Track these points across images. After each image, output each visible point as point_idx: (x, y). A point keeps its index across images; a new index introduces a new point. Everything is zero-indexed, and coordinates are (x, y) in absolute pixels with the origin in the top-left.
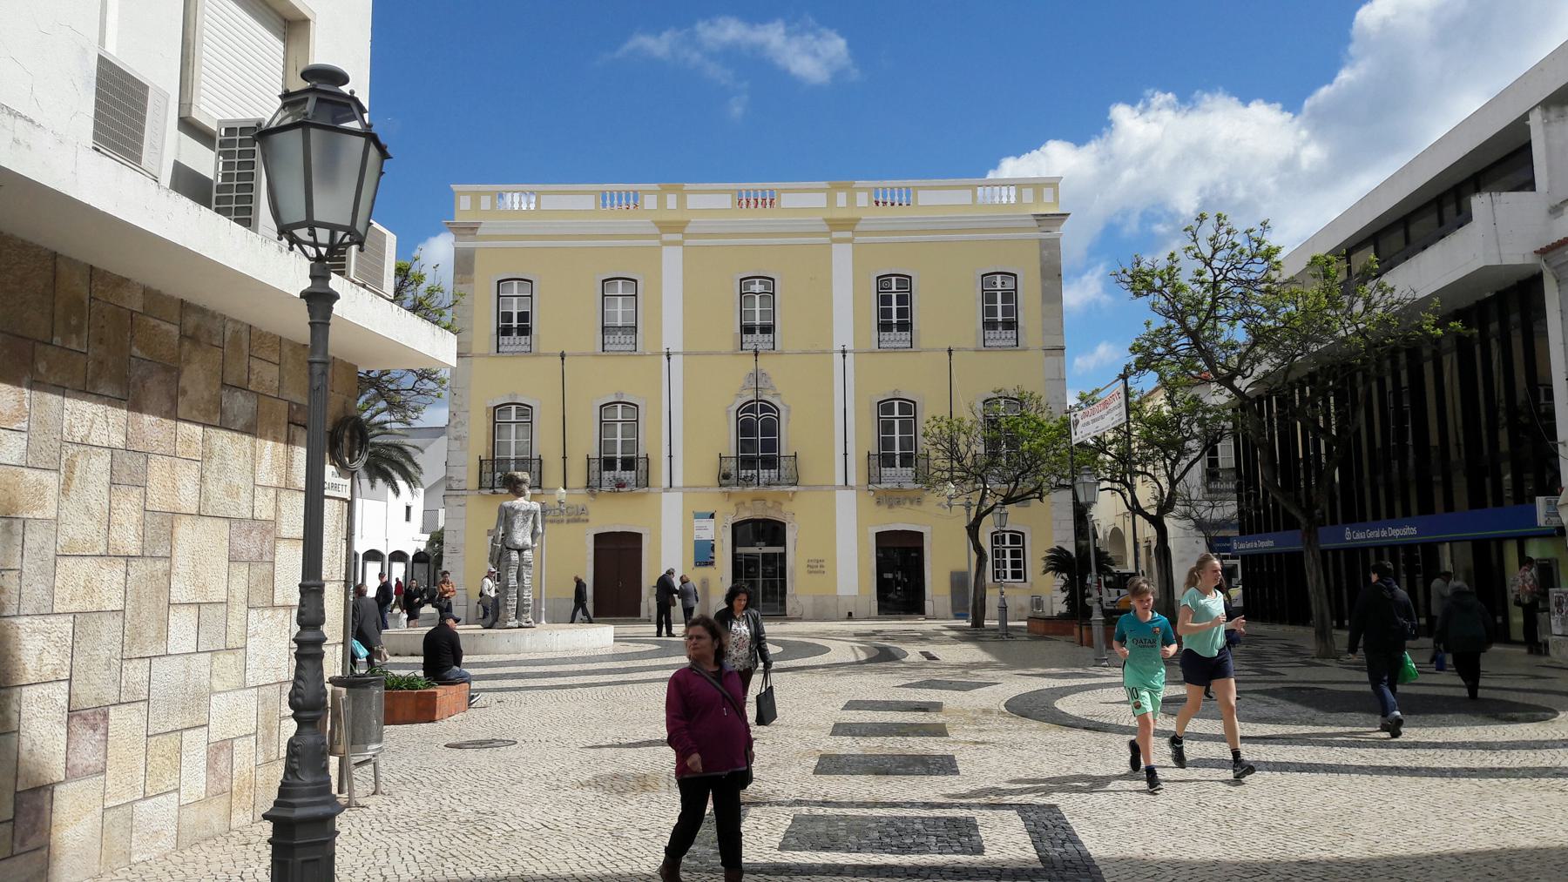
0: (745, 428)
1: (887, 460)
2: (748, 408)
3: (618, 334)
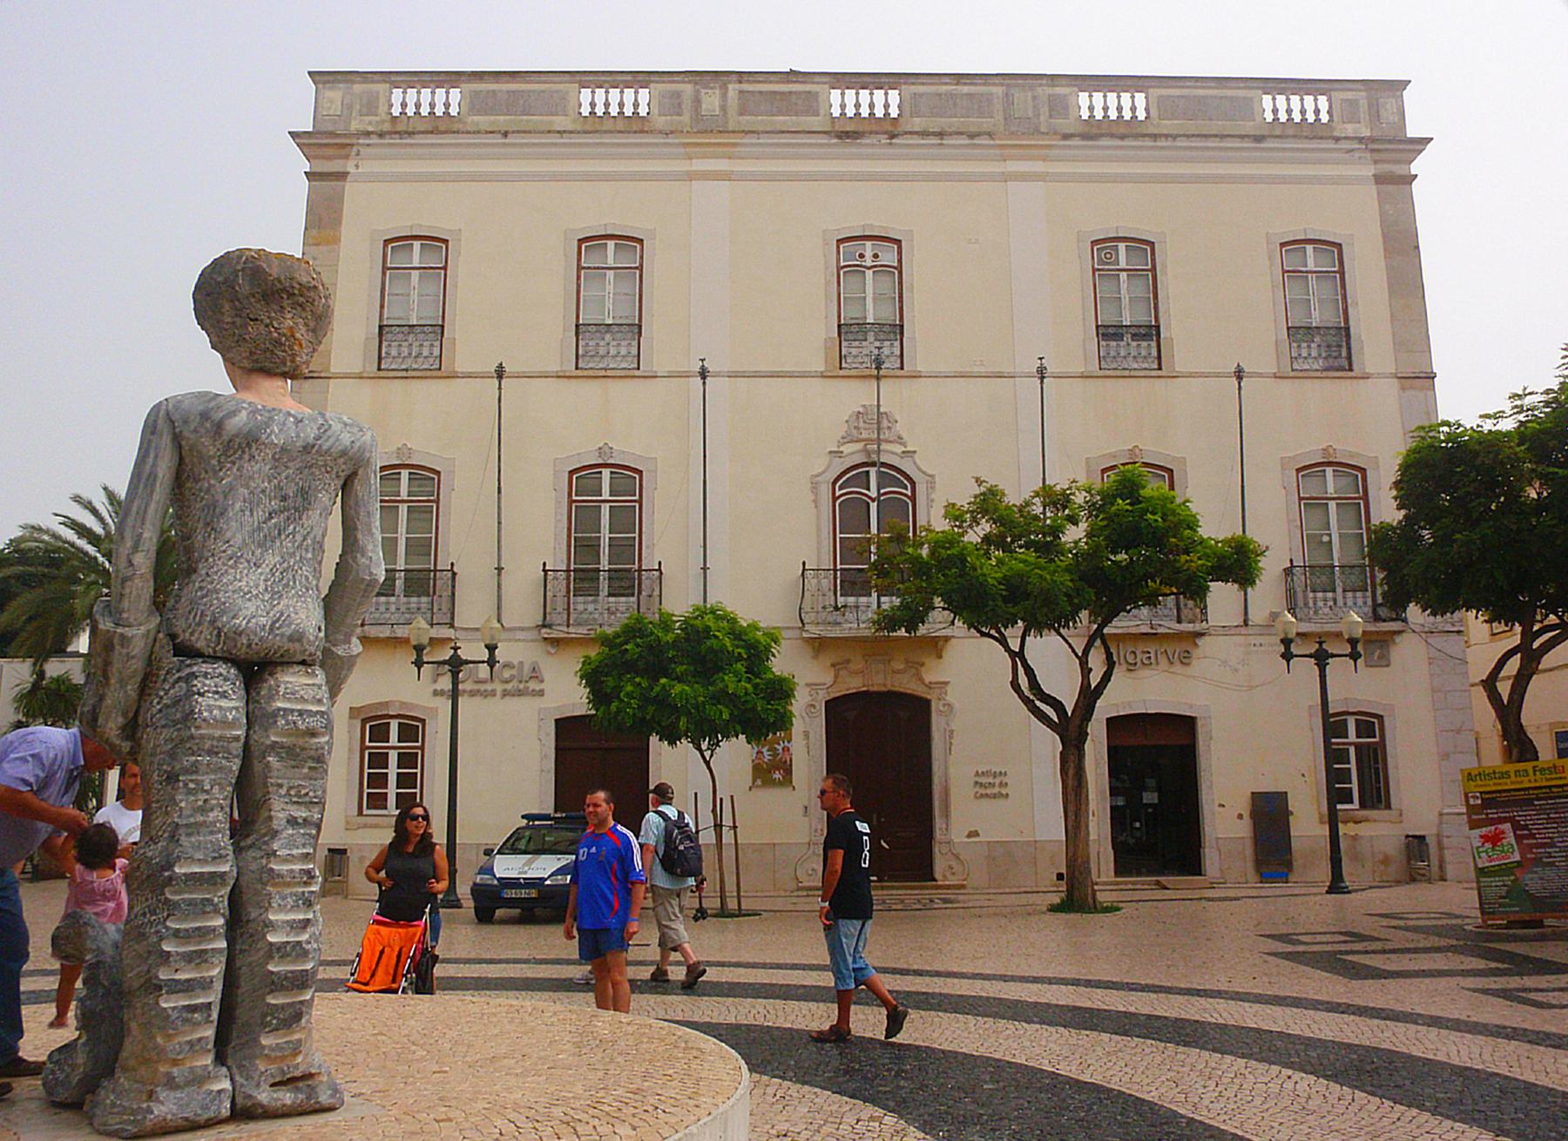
0: (581, 517)
2: (856, 475)
3: (606, 344)
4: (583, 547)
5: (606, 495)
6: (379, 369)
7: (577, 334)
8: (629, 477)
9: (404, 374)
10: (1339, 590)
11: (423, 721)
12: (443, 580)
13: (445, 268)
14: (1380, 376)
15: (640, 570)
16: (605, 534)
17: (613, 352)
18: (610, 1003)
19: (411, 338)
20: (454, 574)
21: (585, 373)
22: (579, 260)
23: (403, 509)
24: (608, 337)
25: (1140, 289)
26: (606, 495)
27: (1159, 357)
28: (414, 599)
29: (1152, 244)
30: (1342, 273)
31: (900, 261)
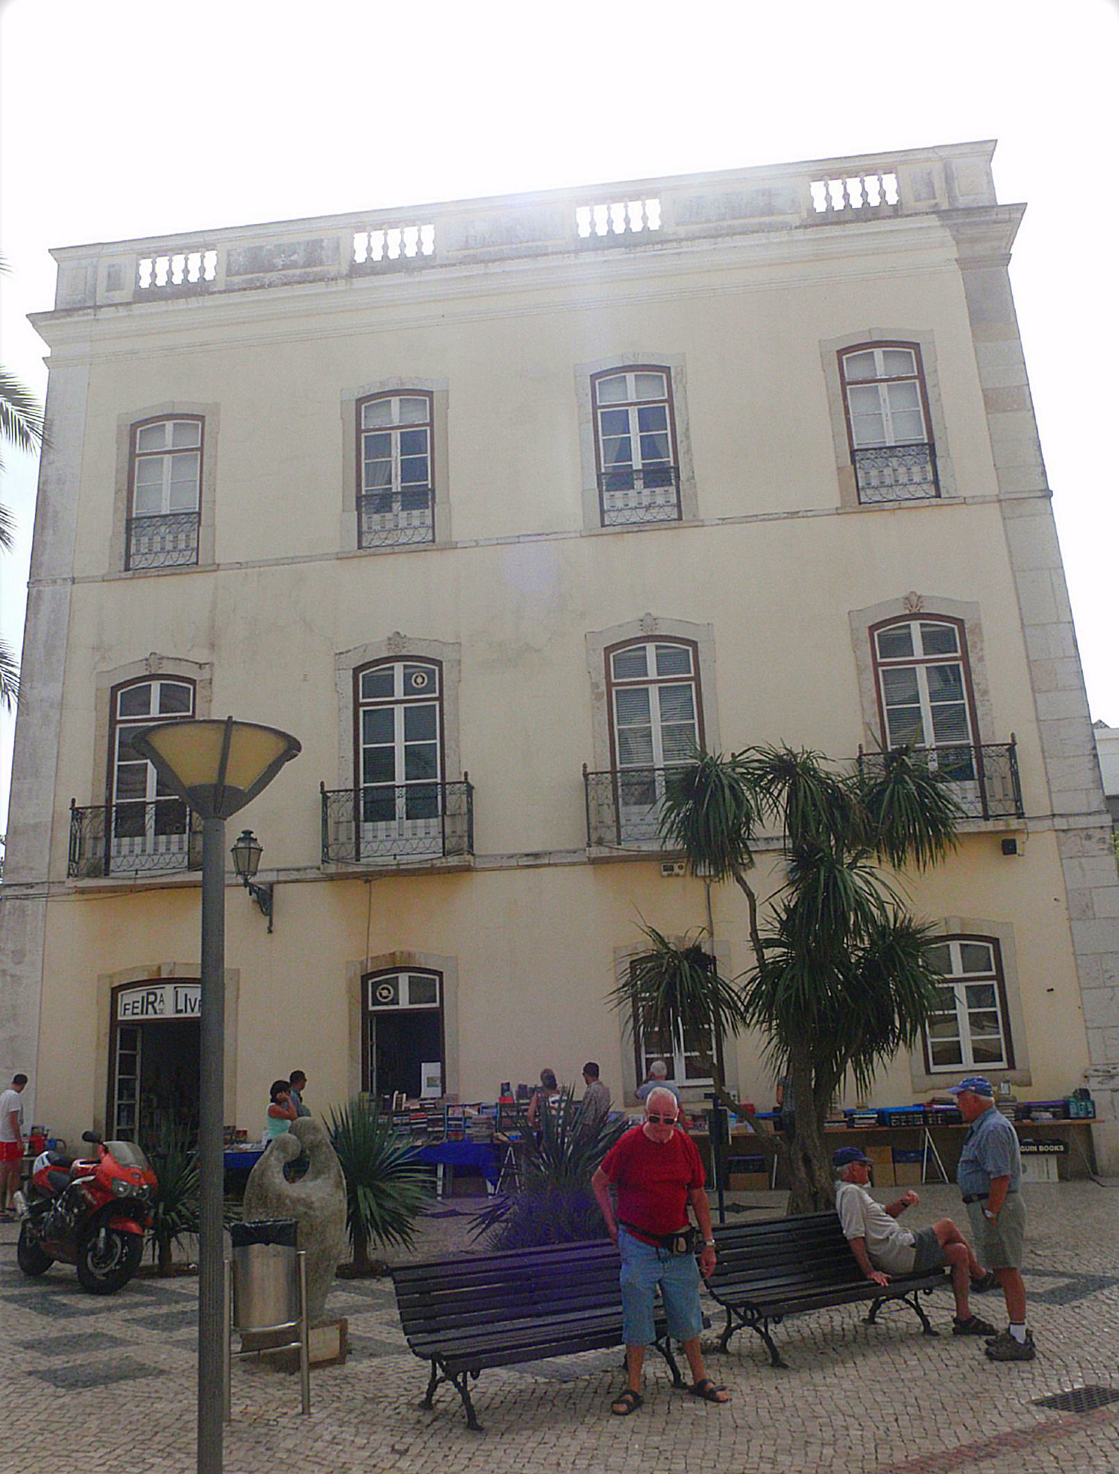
4: (378, 763)
5: (652, 673)
7: (853, 462)
8: (947, 634)
9: (389, 550)
10: (150, 832)
11: (440, 974)
12: (996, 766)
13: (201, 449)
14: (983, 501)
15: (978, 746)
16: (399, 745)
17: (403, 524)
19: (163, 529)
20: (470, 789)
21: (611, 529)
22: (842, 375)
23: (654, 691)
25: (907, 402)
26: (652, 673)
27: (936, 482)
28: (420, 822)
31: (432, 419)
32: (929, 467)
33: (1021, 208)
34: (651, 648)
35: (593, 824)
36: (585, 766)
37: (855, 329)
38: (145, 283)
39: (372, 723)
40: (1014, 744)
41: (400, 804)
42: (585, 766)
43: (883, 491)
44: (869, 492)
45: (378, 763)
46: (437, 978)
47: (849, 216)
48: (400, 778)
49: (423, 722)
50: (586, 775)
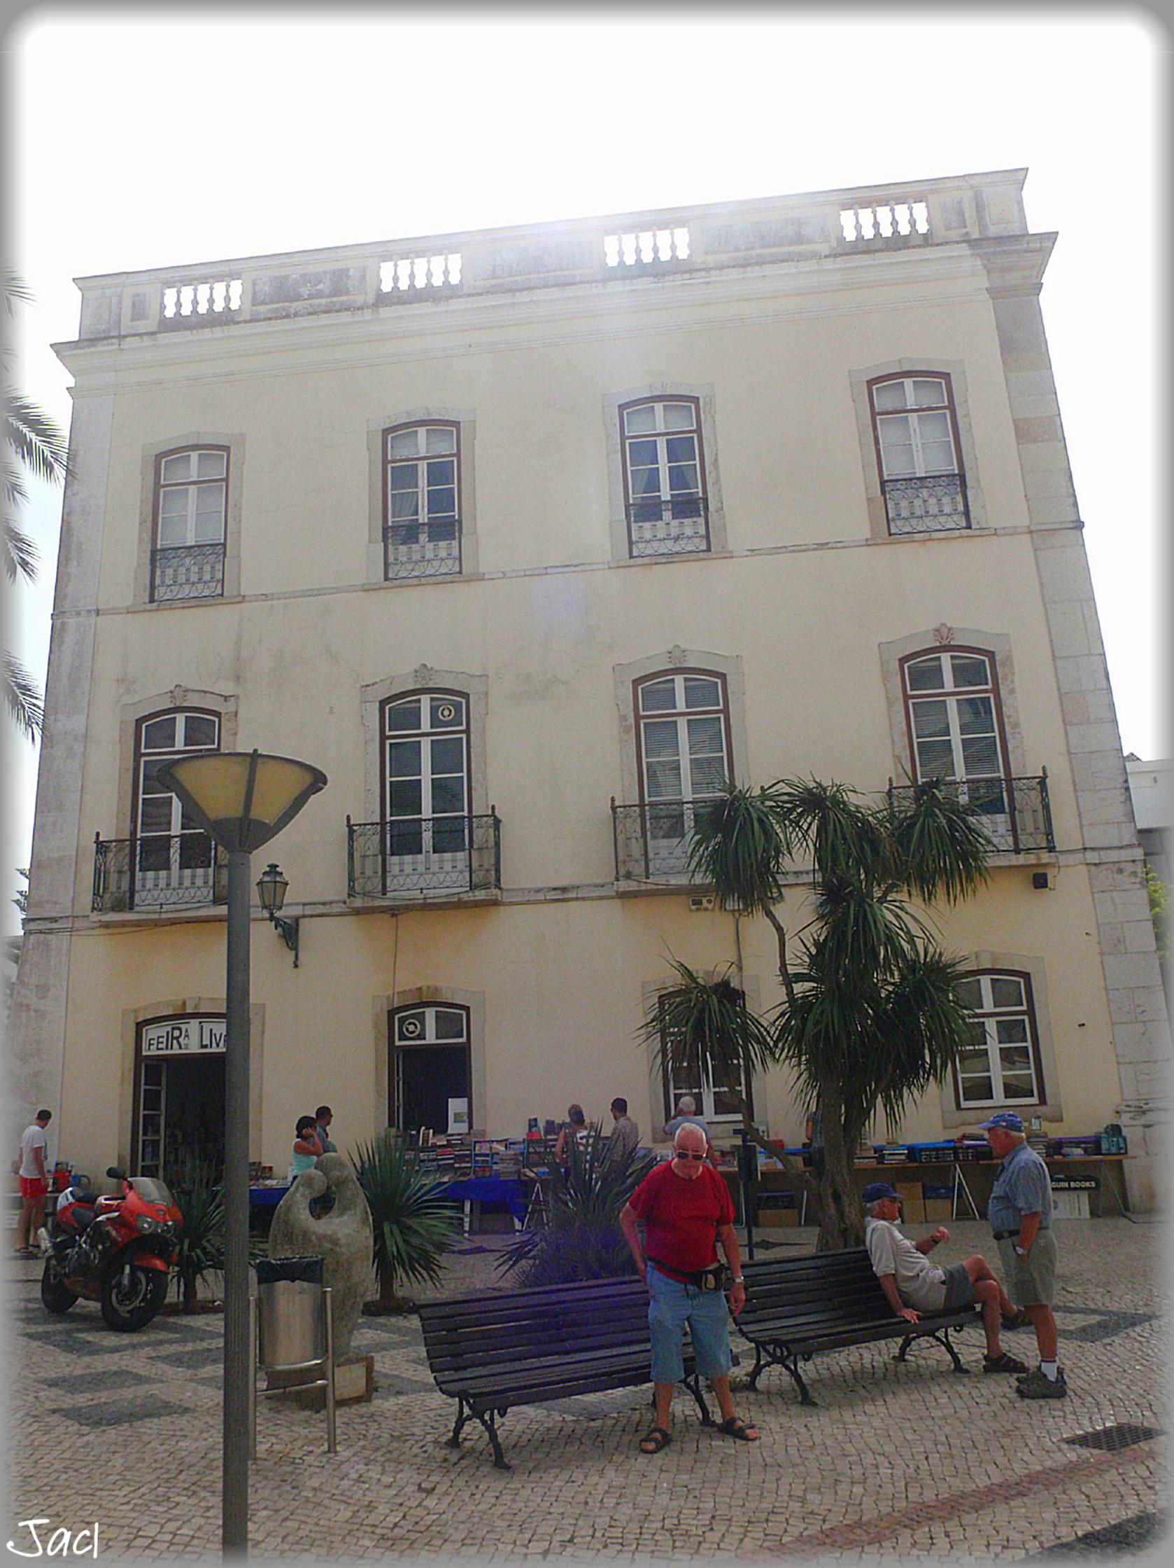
1: (404, 841)
4: (403, 797)
5: (681, 706)
6: (631, 557)
7: (883, 493)
8: (978, 667)
9: (415, 581)
11: (467, 1009)
13: (226, 480)
14: (1014, 532)
15: (1009, 779)
18: (1117, 1443)
20: (497, 822)
21: (639, 561)
23: (682, 724)
24: (924, 493)
25: (938, 433)
26: (681, 706)
27: (708, 537)
29: (946, 376)
30: (951, 407)
31: (459, 450)
32: (959, 498)
33: (1052, 237)
34: (679, 681)
35: (621, 858)
36: (613, 800)
37: (884, 359)
38: (170, 312)
39: (399, 756)
40: (1045, 777)
41: (427, 837)
42: (613, 800)
43: (914, 522)
44: (899, 523)
45: (405, 797)
46: (464, 1013)
47: (880, 245)
48: (427, 811)
49: (450, 755)
50: (614, 809)
